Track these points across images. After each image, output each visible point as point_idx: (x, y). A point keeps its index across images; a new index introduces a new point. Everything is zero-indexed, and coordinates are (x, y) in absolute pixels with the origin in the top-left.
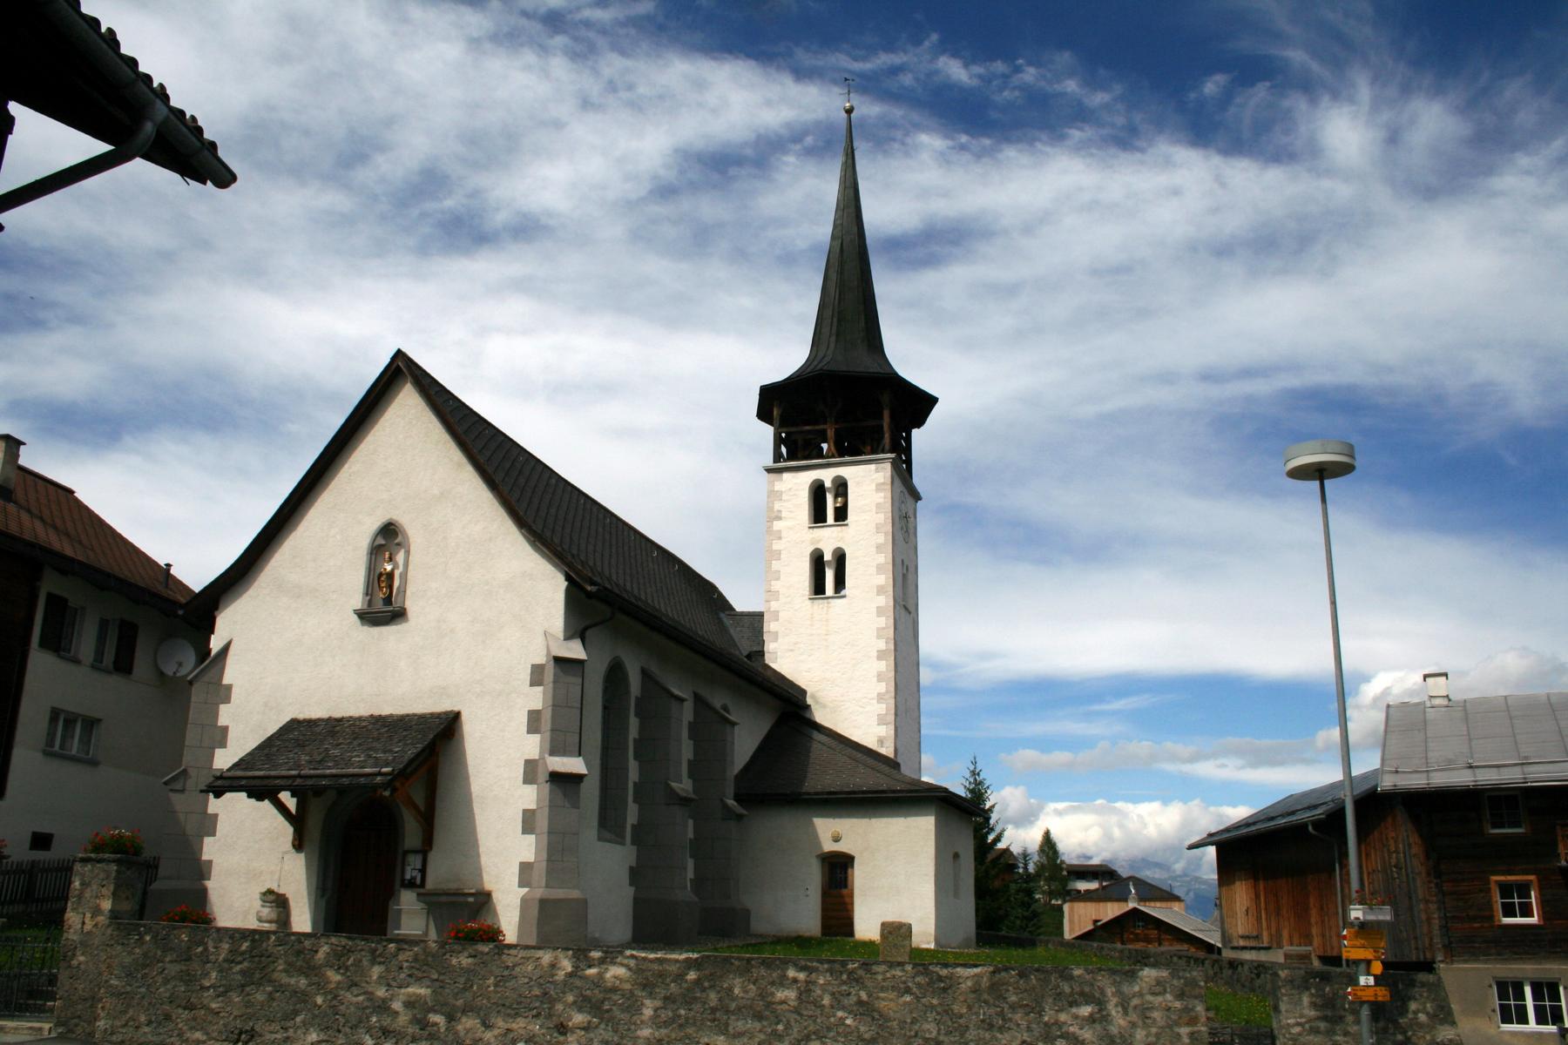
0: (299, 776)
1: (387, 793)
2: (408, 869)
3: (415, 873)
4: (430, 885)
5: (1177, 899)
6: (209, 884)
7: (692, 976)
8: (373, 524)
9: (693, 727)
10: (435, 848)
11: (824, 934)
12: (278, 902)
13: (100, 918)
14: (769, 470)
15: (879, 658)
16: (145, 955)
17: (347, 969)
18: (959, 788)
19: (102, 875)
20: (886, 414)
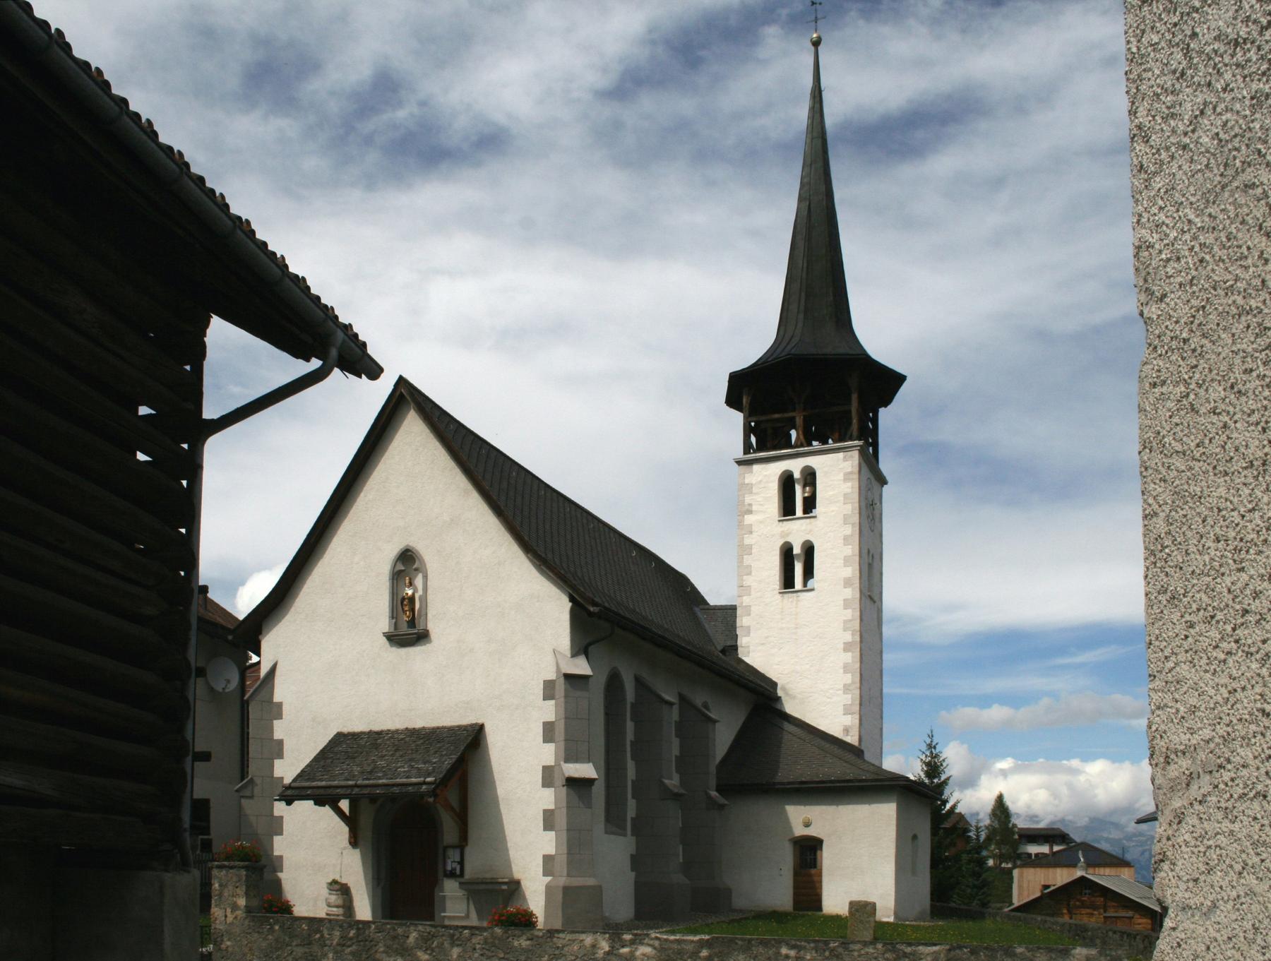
0: (356, 786)
1: (431, 800)
2: (449, 862)
3: (455, 865)
4: (468, 874)
5: (1127, 864)
6: (282, 875)
7: (704, 953)
8: (392, 551)
9: (680, 727)
10: (470, 842)
11: (795, 908)
12: (341, 890)
13: (239, 912)
14: (740, 463)
15: (845, 650)
16: (277, 940)
17: (433, 950)
18: (914, 770)
19: (235, 879)
20: (855, 397)
